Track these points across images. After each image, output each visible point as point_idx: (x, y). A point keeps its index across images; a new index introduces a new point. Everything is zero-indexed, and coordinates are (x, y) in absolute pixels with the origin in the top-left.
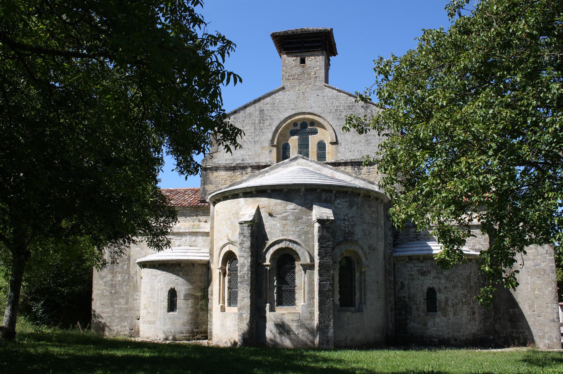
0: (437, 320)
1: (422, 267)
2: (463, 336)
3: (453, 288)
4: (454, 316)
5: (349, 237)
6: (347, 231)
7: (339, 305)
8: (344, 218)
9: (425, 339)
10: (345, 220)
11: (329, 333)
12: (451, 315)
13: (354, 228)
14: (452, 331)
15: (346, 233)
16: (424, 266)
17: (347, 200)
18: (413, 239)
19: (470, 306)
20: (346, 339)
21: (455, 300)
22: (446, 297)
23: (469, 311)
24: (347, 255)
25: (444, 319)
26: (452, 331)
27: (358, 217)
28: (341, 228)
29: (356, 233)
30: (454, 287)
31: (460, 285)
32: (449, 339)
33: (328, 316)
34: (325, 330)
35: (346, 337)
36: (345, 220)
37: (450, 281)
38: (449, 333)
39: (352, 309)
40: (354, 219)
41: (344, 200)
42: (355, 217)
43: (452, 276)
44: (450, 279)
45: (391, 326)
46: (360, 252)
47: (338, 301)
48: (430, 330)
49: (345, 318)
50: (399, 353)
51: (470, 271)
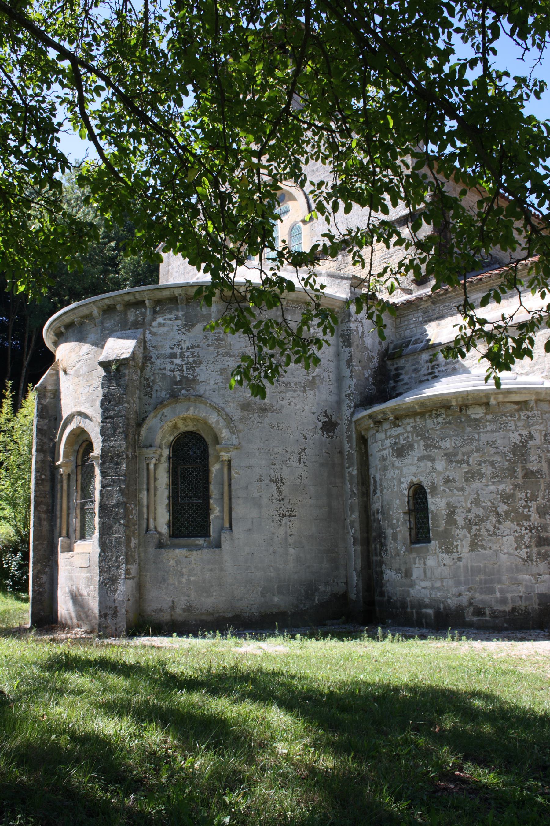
0: (431, 562)
1: (397, 437)
2: (504, 601)
3: (466, 480)
4: (472, 550)
5: (182, 389)
6: (178, 378)
7: (167, 535)
8: (173, 351)
9: (409, 610)
10: (173, 356)
11: (118, 592)
12: (464, 548)
13: (197, 370)
14: (469, 590)
15: (176, 383)
16: (400, 434)
17: (180, 314)
18: (425, 378)
19: (526, 524)
20: (173, 607)
21: (475, 509)
22: (448, 504)
23: (522, 537)
24: (187, 429)
25: (447, 559)
26: (469, 590)
27: (208, 345)
28: (163, 374)
29: (200, 379)
30: (470, 476)
31: (487, 470)
32: (459, 612)
33: (117, 558)
34: (110, 587)
35: (173, 602)
36: (173, 356)
37: (457, 462)
38: (460, 595)
39: (201, 541)
40: (196, 350)
41: (173, 316)
42: (198, 346)
43: (464, 450)
44: (460, 457)
45: (355, 578)
46: (213, 419)
47: (166, 527)
48: (417, 587)
49: (172, 562)
50: (508, 643)
51: (525, 433)
